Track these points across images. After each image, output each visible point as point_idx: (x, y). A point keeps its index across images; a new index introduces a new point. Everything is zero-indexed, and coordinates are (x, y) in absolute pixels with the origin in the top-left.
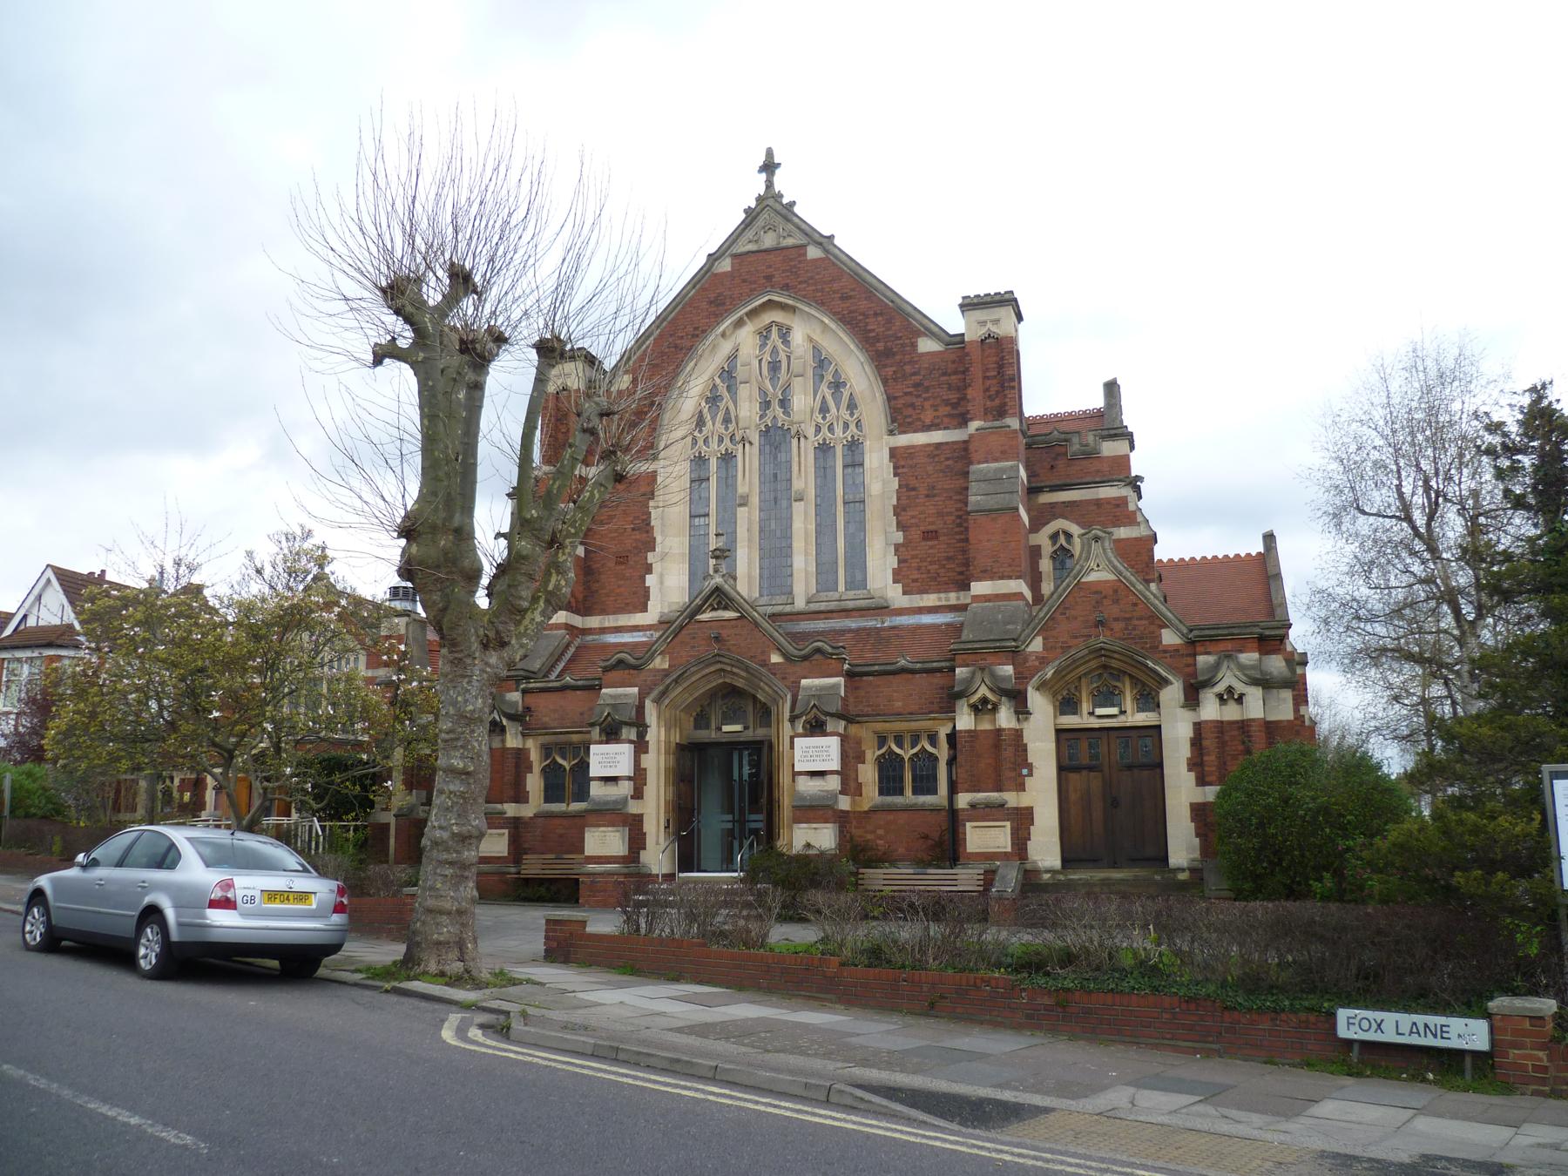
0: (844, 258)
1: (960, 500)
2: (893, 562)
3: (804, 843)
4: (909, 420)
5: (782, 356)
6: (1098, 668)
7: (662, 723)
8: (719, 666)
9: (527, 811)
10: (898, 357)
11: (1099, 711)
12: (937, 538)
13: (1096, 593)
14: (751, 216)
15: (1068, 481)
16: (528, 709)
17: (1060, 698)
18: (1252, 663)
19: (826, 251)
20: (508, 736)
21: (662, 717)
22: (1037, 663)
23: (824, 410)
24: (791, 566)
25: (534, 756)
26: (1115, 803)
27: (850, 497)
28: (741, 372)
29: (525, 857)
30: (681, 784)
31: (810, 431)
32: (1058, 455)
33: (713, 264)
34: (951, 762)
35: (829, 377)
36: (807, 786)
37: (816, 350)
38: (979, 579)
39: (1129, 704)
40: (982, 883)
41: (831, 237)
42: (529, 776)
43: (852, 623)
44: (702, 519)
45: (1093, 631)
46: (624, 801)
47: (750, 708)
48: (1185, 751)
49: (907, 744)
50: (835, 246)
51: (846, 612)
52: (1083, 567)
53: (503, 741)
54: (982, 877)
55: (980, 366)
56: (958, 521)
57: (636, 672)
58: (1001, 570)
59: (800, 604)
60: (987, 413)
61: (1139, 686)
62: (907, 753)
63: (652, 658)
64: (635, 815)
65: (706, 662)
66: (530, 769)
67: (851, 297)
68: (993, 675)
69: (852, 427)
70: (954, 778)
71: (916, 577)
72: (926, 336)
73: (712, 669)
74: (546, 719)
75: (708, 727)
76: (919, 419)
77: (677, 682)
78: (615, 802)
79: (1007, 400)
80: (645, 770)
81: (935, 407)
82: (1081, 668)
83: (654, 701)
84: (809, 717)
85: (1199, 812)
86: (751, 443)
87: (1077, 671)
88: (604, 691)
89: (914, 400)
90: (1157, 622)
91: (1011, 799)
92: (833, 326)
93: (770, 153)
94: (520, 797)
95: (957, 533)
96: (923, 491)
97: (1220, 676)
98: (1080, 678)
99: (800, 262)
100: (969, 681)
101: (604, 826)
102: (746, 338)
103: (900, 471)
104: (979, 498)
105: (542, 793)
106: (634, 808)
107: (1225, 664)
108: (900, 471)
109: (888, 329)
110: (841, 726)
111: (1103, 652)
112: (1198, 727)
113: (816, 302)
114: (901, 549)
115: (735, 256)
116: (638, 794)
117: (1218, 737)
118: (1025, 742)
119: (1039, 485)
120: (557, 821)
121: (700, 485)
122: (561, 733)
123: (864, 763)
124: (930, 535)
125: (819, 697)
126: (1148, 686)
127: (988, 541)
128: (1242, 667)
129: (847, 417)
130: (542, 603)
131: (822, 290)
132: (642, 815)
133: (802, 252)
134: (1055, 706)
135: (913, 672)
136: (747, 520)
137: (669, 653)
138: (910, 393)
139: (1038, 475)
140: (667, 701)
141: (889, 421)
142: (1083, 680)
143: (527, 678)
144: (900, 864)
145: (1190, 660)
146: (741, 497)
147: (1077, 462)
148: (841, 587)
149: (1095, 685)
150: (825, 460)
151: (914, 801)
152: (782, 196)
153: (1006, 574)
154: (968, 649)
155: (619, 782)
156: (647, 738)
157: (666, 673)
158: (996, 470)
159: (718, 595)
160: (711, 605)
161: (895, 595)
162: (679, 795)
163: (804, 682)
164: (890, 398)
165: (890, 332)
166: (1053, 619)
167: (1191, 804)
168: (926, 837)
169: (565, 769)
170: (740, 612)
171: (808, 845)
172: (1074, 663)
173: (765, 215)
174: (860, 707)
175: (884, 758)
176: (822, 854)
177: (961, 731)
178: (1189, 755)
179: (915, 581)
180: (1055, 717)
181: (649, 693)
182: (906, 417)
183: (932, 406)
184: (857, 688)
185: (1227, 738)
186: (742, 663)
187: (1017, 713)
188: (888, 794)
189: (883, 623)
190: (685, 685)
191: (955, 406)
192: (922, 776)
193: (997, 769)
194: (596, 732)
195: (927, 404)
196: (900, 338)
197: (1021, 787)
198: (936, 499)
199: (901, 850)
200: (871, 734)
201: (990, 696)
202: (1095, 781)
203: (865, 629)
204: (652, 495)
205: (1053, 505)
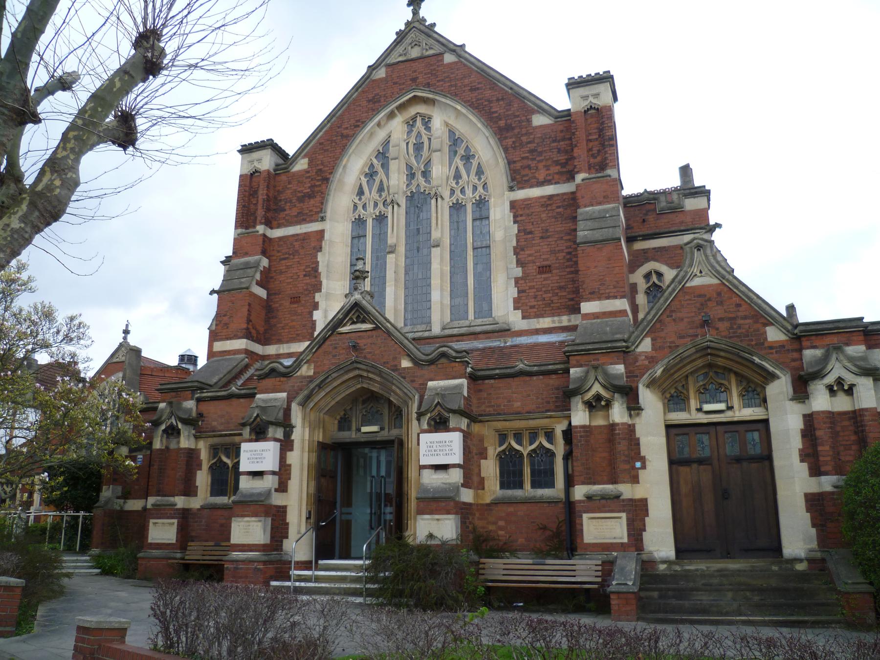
0: (473, 60)
1: (570, 240)
2: (513, 292)
3: (427, 533)
4: (526, 178)
5: (425, 139)
6: (703, 367)
7: (307, 424)
8: (357, 372)
9: (195, 503)
10: (516, 131)
11: (707, 407)
12: (550, 272)
13: (700, 296)
14: (401, 36)
15: (657, 231)
16: (200, 415)
17: (668, 396)
18: (860, 355)
19: (459, 56)
20: (182, 439)
21: (307, 419)
22: (646, 362)
23: (457, 176)
24: (430, 301)
25: (204, 455)
26: (725, 495)
27: (479, 244)
28: (392, 152)
30: (323, 480)
31: (446, 194)
32: (648, 211)
33: (371, 73)
34: (568, 456)
35: (461, 151)
36: (431, 479)
37: (452, 133)
38: (588, 300)
39: (736, 401)
40: (600, 574)
41: (462, 46)
42: (199, 473)
43: (479, 344)
45: (699, 331)
46: (268, 493)
47: (386, 412)
48: (796, 443)
49: (525, 441)
50: (466, 52)
51: (474, 335)
52: (687, 272)
53: (179, 442)
54: (600, 568)
55: (584, 130)
56: (568, 257)
57: (285, 379)
58: (607, 291)
59: (436, 330)
60: (590, 168)
61: (744, 384)
62: (525, 450)
64: (279, 507)
65: (346, 369)
66: (200, 467)
67: (478, 89)
68: (606, 374)
69: (480, 189)
70: (570, 472)
71: (532, 304)
72: (539, 112)
73: (351, 375)
74: (214, 424)
75: (349, 429)
76: (535, 177)
78: (260, 494)
79: (607, 155)
80: (290, 466)
81: (547, 168)
82: (688, 367)
84: (433, 414)
85: (814, 502)
86: (398, 205)
87: (684, 370)
88: (258, 396)
89: (530, 162)
90: (762, 320)
91: (626, 490)
92: (464, 111)
94: (189, 490)
95: (567, 267)
96: (538, 234)
97: (829, 367)
98: (687, 376)
100: (583, 379)
102: (397, 127)
103: (519, 219)
104: (586, 233)
106: (278, 500)
107: (834, 356)
109: (510, 110)
110: (464, 423)
111: (709, 351)
112: (809, 419)
113: (451, 94)
115: (388, 66)
116: (282, 487)
117: (831, 428)
118: (637, 436)
119: (633, 234)
121: (359, 241)
122: (226, 435)
123: (486, 458)
124: (544, 269)
125: (443, 396)
126: (753, 382)
127: (596, 267)
128: (851, 359)
129: (476, 181)
130: (24, 207)
131: (456, 86)
132: (285, 507)
133: (440, 58)
134: (664, 404)
135: (530, 374)
136: (395, 264)
137: (314, 362)
138: (527, 158)
139: (632, 228)
140: (312, 405)
141: (510, 180)
142: (690, 378)
143: (201, 389)
144: (520, 554)
145: (795, 355)
146: (391, 246)
147: (665, 216)
148: (471, 316)
149: (701, 383)
150: (458, 216)
151: (532, 494)
152: (425, 21)
153: (611, 294)
154: (582, 350)
155: (265, 476)
156: (293, 437)
157: (311, 379)
158: (599, 211)
159: (357, 310)
160: (351, 319)
161: (516, 320)
162: (319, 489)
163: (431, 384)
164: (510, 163)
165: (510, 112)
166: (660, 321)
168: (544, 528)
169: (228, 467)
170: (376, 324)
171: (431, 536)
172: (682, 362)
173: (412, 35)
174: (483, 408)
175: (505, 454)
176: (444, 543)
177: (576, 427)
178: (801, 446)
179: (532, 307)
180: (665, 414)
181: (295, 397)
182: (524, 176)
183: (545, 166)
184: (480, 391)
185: (838, 429)
186: (376, 368)
187: (629, 409)
188: (509, 488)
189: (506, 343)
190: (328, 390)
191: (564, 165)
192: (540, 471)
193: (612, 463)
194: (246, 431)
195: (541, 166)
196: (518, 116)
197: (635, 480)
198: (550, 240)
199: (521, 541)
200: (493, 433)
201: (603, 392)
202: (705, 475)
203: (490, 348)
204: (320, 249)
205: (645, 251)
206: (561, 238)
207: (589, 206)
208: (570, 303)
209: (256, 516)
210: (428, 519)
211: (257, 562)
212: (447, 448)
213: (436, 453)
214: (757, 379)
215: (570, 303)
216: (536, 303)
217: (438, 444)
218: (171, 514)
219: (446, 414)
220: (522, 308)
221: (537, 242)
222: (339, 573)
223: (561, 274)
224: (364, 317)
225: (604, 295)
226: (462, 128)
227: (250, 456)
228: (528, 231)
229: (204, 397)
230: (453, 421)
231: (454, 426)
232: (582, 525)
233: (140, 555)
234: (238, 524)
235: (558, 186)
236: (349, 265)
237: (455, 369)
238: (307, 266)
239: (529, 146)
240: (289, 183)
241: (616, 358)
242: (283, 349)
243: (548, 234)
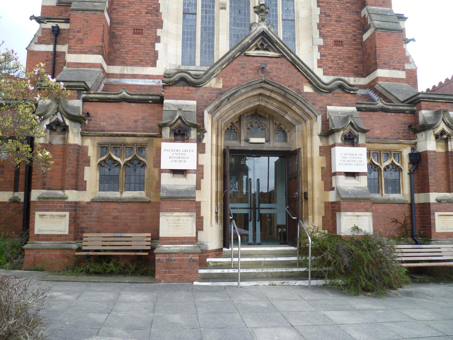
1: (355, 26)
3: (353, 226)
8: (261, 91)
12: (342, 45)
25: (92, 152)
29: (85, 235)
38: (382, 68)
44: (191, 16)
53: (65, 139)
56: (354, 38)
57: (194, 88)
58: (394, 64)
63: (209, 78)
65: (253, 87)
66: (87, 163)
75: (238, 138)
77: (229, 100)
83: (210, 112)
95: (353, 44)
96: (334, 18)
101: (179, 211)
105: (98, 183)
108: (320, 4)
114: (322, 49)
120: (113, 206)
122: (117, 135)
124: (338, 43)
137: (222, 77)
151: (387, 197)
153: (397, 67)
157: (221, 92)
160: (256, 45)
171: (356, 228)
194: (166, 132)
201: (447, 129)
206: (350, 24)
207: (373, 6)
208: (355, 69)
209: (187, 211)
210: (350, 216)
211: (193, 253)
212: (358, 160)
213: (349, 163)
215: (355, 69)
216: (332, 65)
217: (350, 156)
218: (60, 206)
219: (356, 133)
220: (323, 67)
221: (333, 23)
222: (254, 259)
223: (349, 48)
224: (269, 45)
225: (392, 67)
227: (171, 156)
228: (327, 14)
229: (92, 98)
230: (362, 139)
231: (362, 142)
232: (434, 220)
233: (26, 247)
234: (166, 218)
236: (182, 13)
237: (348, 99)
238: (149, 6)
241: (450, 107)
242: (127, 70)
243: (341, 19)
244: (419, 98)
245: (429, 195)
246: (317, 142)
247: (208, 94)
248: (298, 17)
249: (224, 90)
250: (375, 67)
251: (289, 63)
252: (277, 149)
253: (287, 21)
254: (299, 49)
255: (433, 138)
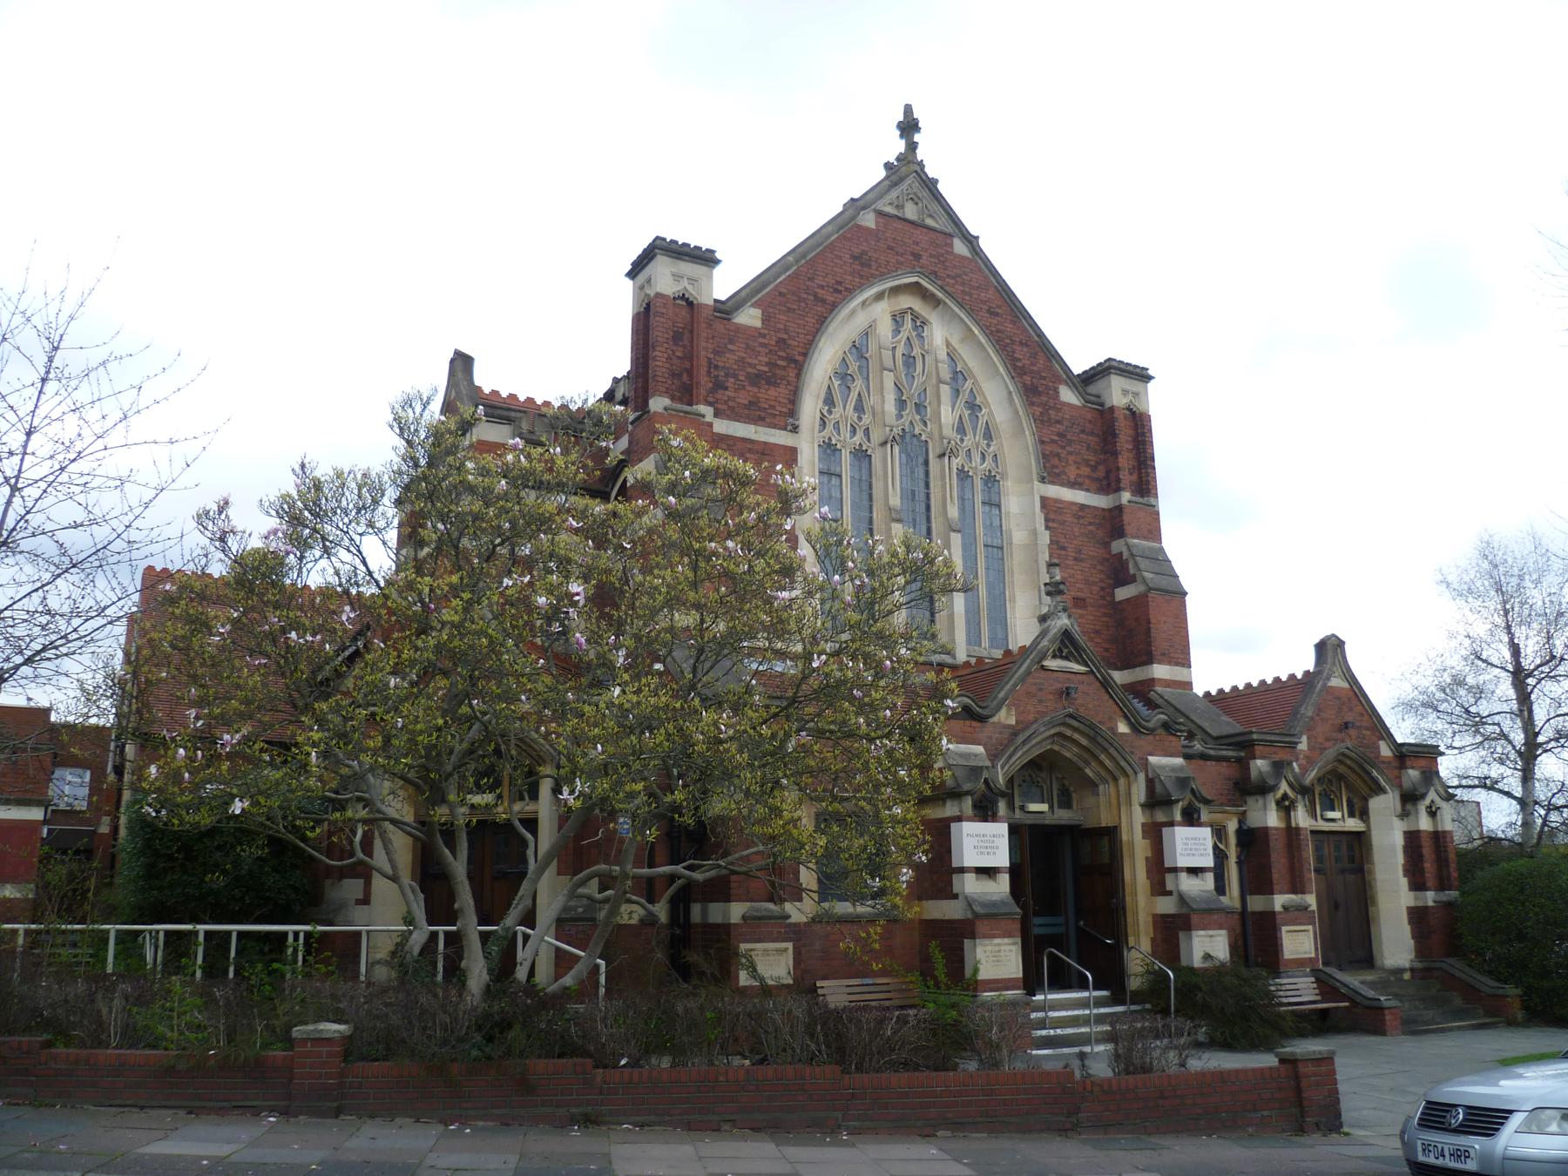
3: (1202, 954)
4: (1057, 471)
10: (1044, 399)
37: (952, 356)
38: (1160, 662)
41: (977, 238)
56: (1101, 593)
57: (979, 724)
69: (989, 459)
85: (1418, 916)
92: (983, 339)
93: (908, 110)
99: (947, 252)
108: (1050, 524)
131: (971, 295)
138: (1053, 441)
167: (1408, 908)
183: (1075, 462)
194: (968, 803)
196: (1044, 378)
210: (1201, 936)
214: (1364, 790)
221: (1070, 563)
224: (1070, 652)
226: (970, 359)
235: (1088, 494)
239: (1058, 426)
240: (731, 341)
244: (1254, 740)
245: (1273, 899)
246: (1139, 817)
247: (997, 736)
248: (1011, 543)
249: (1019, 728)
250: (1150, 660)
251: (1098, 684)
252: (1063, 822)
253: (990, 549)
254: (1014, 608)
255: (1273, 806)
